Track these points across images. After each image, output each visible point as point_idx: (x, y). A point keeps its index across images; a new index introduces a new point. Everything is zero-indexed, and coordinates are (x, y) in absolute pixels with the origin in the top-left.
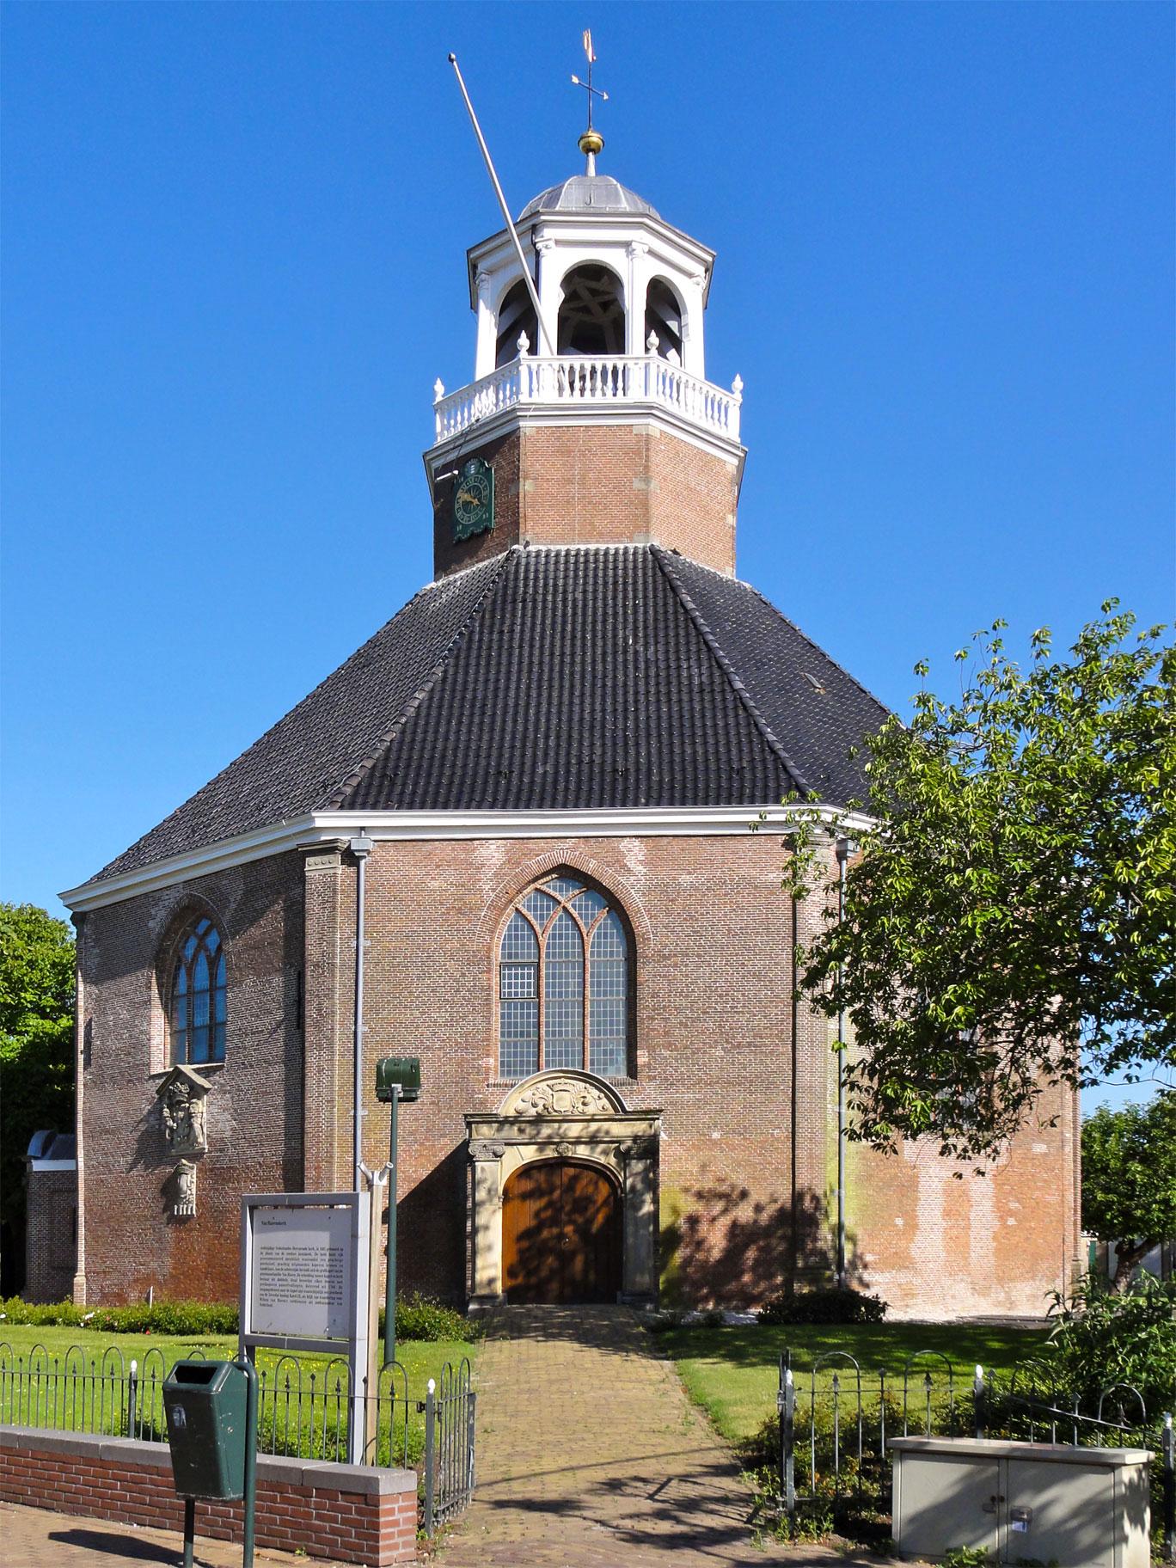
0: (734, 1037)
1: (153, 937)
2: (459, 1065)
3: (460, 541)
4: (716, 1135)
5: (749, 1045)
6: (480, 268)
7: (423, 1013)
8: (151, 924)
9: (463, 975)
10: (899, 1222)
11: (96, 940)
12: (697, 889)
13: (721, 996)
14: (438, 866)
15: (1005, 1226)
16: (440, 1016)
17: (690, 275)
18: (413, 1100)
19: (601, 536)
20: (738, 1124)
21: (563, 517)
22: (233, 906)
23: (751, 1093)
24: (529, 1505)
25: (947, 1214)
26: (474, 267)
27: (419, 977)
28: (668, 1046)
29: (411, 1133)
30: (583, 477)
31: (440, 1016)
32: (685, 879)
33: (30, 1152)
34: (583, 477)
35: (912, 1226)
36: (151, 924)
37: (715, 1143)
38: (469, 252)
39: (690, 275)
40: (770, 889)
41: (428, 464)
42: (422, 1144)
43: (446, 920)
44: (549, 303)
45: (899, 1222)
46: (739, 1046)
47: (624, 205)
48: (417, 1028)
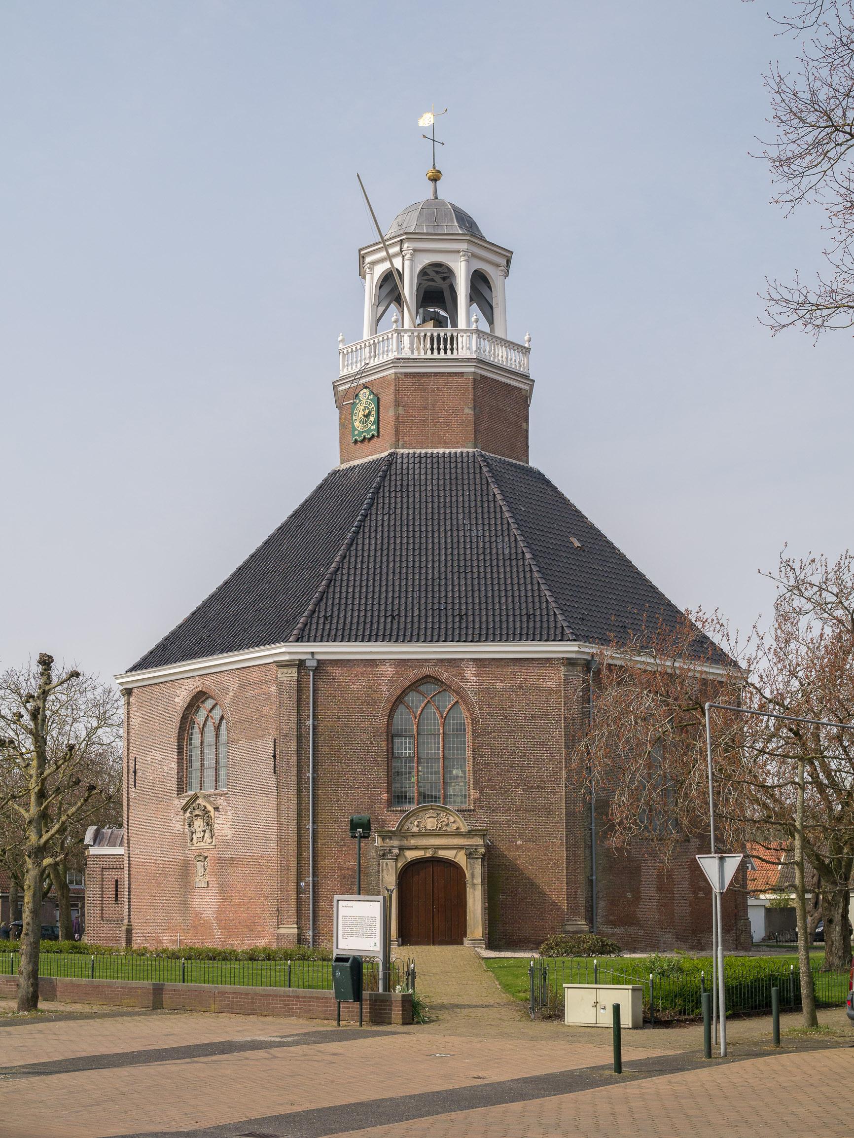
0: (529, 782)
1: (178, 708)
2: (370, 798)
3: (356, 442)
4: (519, 842)
5: (538, 787)
6: (368, 259)
7: (348, 766)
8: (177, 700)
9: (371, 743)
10: (629, 895)
11: (139, 707)
12: (506, 691)
13: (521, 757)
14: (356, 676)
15: (696, 897)
16: (358, 768)
17: (498, 266)
18: (367, 837)
19: (445, 444)
20: (532, 835)
21: (421, 431)
22: (231, 694)
23: (540, 817)
24: (470, 1006)
25: (659, 890)
26: (362, 258)
27: (346, 744)
28: (491, 787)
29: (342, 840)
30: (434, 406)
31: (358, 768)
32: (499, 685)
33: (86, 841)
34: (434, 406)
35: (637, 898)
36: (177, 700)
37: (518, 847)
38: (360, 251)
39: (498, 266)
40: (551, 691)
41: (335, 388)
42: (348, 847)
43: (361, 709)
44: (408, 289)
45: (629, 895)
46: (532, 787)
47: (460, 232)
48: (345, 775)
